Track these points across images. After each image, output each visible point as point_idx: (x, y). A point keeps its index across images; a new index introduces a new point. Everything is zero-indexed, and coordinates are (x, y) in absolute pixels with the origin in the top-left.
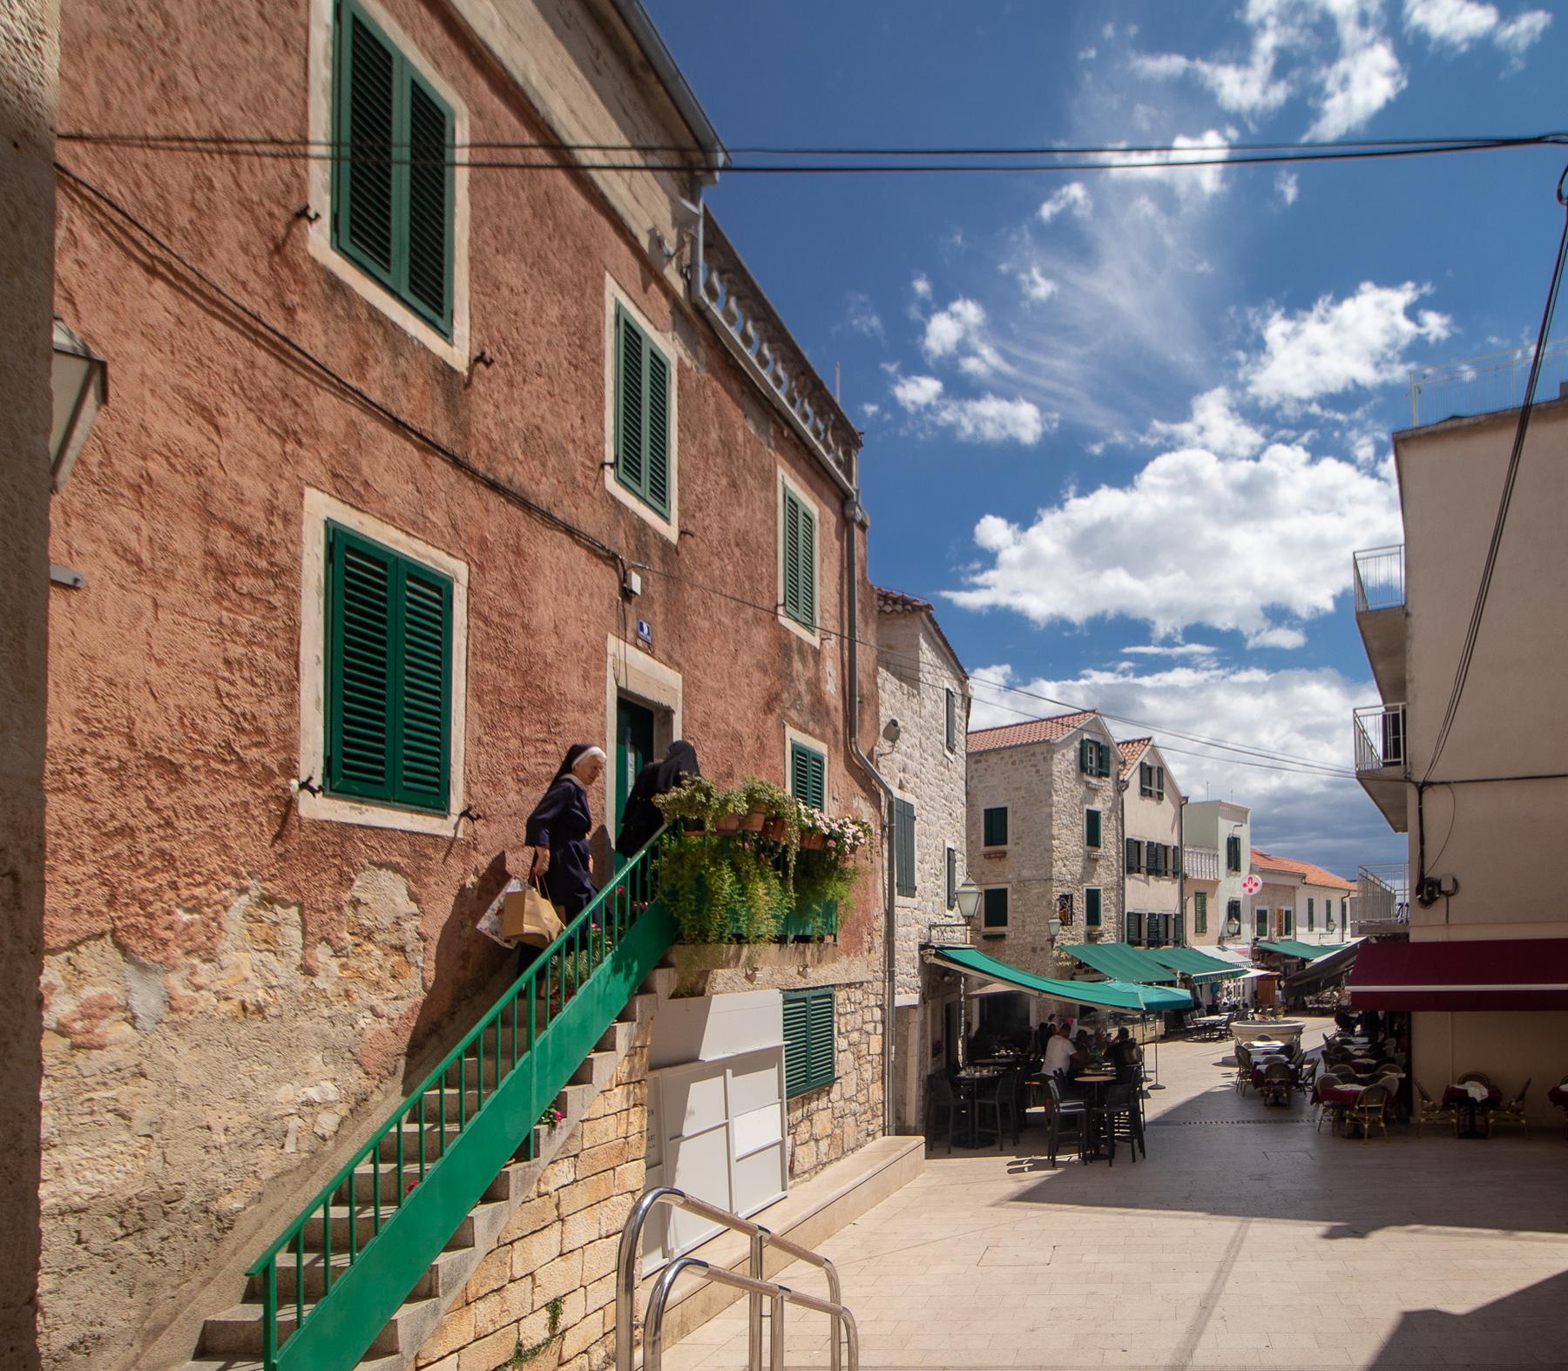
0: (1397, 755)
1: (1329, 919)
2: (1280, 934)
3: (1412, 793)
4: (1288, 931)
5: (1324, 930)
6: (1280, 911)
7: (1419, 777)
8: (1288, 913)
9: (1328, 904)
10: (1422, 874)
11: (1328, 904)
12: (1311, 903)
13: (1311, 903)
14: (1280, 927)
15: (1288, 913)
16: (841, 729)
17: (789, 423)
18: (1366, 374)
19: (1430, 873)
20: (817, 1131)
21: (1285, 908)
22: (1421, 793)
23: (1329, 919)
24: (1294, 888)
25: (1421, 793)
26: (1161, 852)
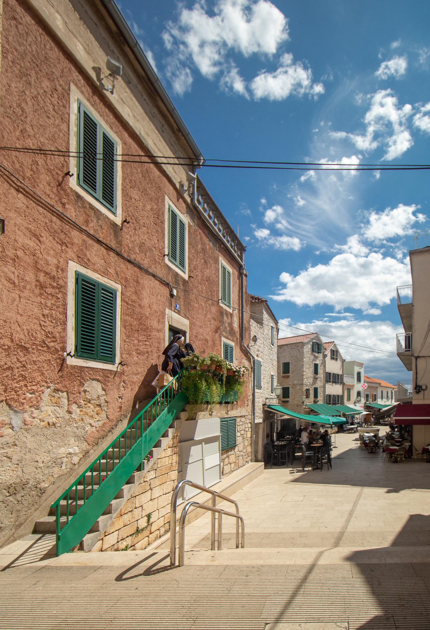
1: (387, 397)
3: (414, 360)
7: (416, 355)
8: (375, 395)
10: (416, 384)
12: (382, 392)
13: (382, 392)
19: (419, 384)
21: (374, 393)
22: (416, 359)
23: (387, 397)
24: (377, 387)
25: (416, 359)
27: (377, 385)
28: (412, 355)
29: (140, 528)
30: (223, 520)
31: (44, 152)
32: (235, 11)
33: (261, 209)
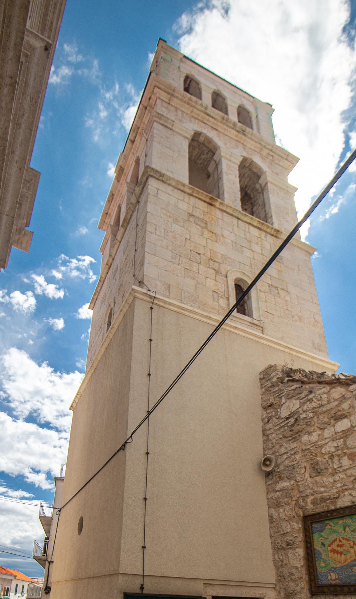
0: (45, 553)
1: (23, 591)
2: (4, 595)
3: (47, 563)
4: (7, 595)
5: (20, 595)
6: (5, 588)
7: (49, 560)
8: (8, 589)
9: (23, 586)
10: (47, 585)
11: (23, 586)
12: (17, 586)
13: (17, 586)
14: (4, 593)
15: (8, 589)
16: (14, 170)
17: (32, 33)
18: (307, 372)
19: (49, 585)
20: (208, 280)
21: (7, 587)
22: (49, 564)
23: (23, 591)
24: (11, 580)
25: (49, 564)
26: (92, 308)
27: (12, 578)
28: (46, 560)
29: (40, 554)
30: (122, 558)
31: (168, 90)
32: (270, 595)
33: (58, 265)
